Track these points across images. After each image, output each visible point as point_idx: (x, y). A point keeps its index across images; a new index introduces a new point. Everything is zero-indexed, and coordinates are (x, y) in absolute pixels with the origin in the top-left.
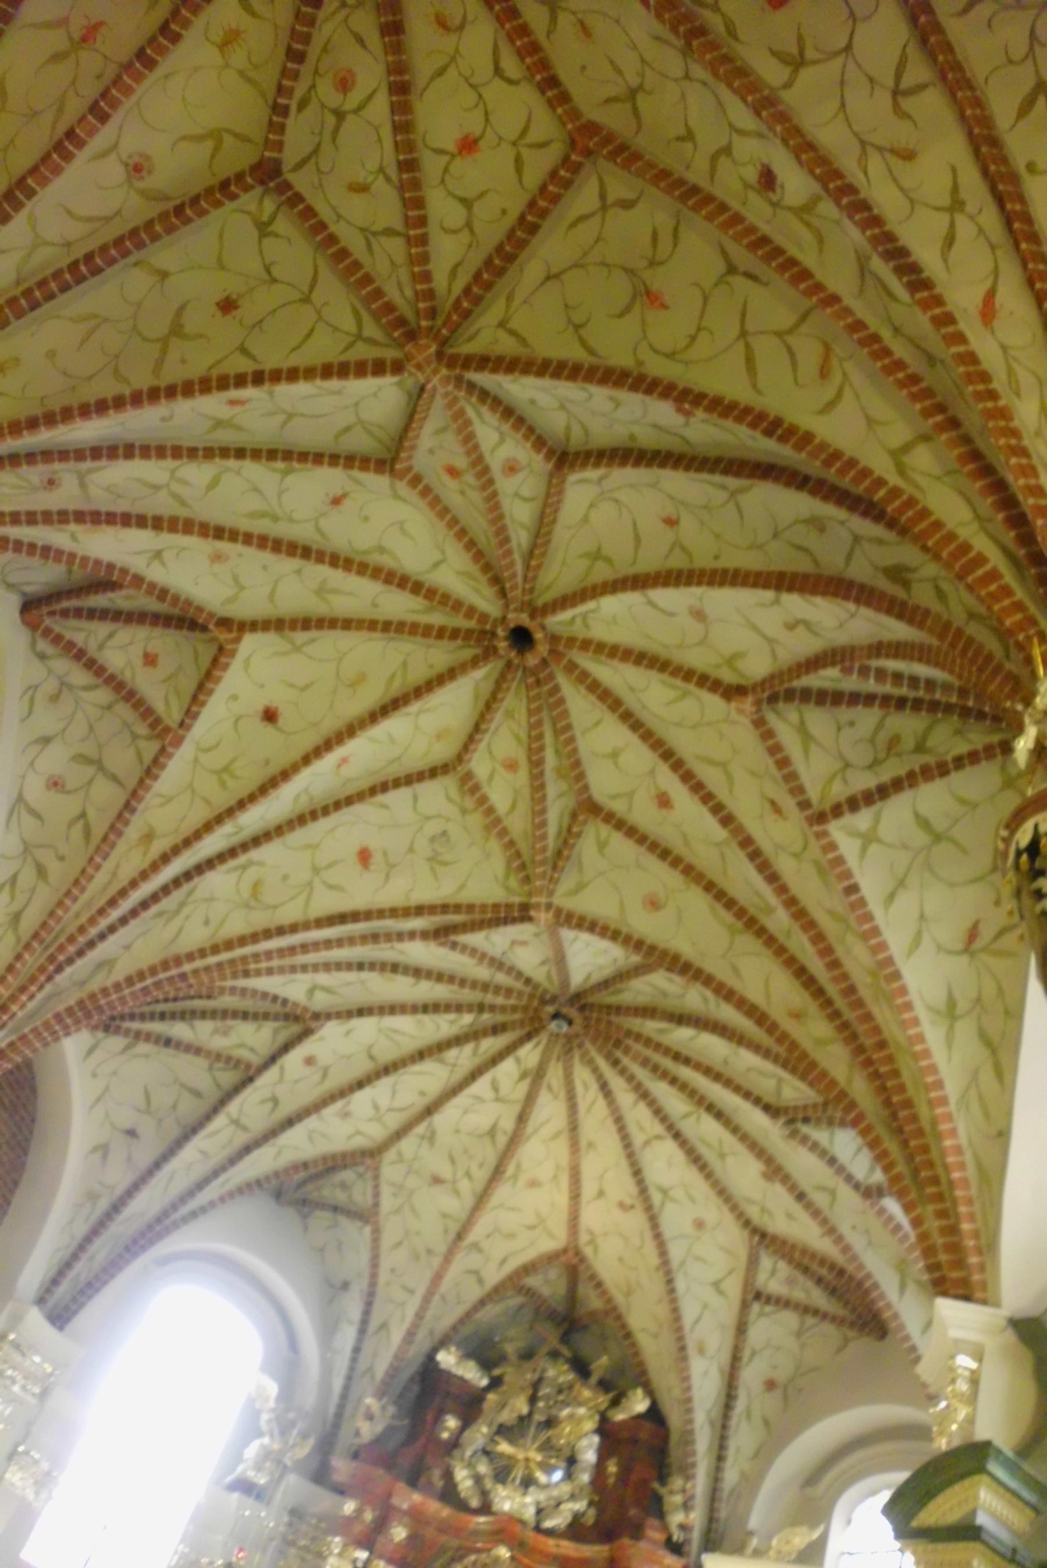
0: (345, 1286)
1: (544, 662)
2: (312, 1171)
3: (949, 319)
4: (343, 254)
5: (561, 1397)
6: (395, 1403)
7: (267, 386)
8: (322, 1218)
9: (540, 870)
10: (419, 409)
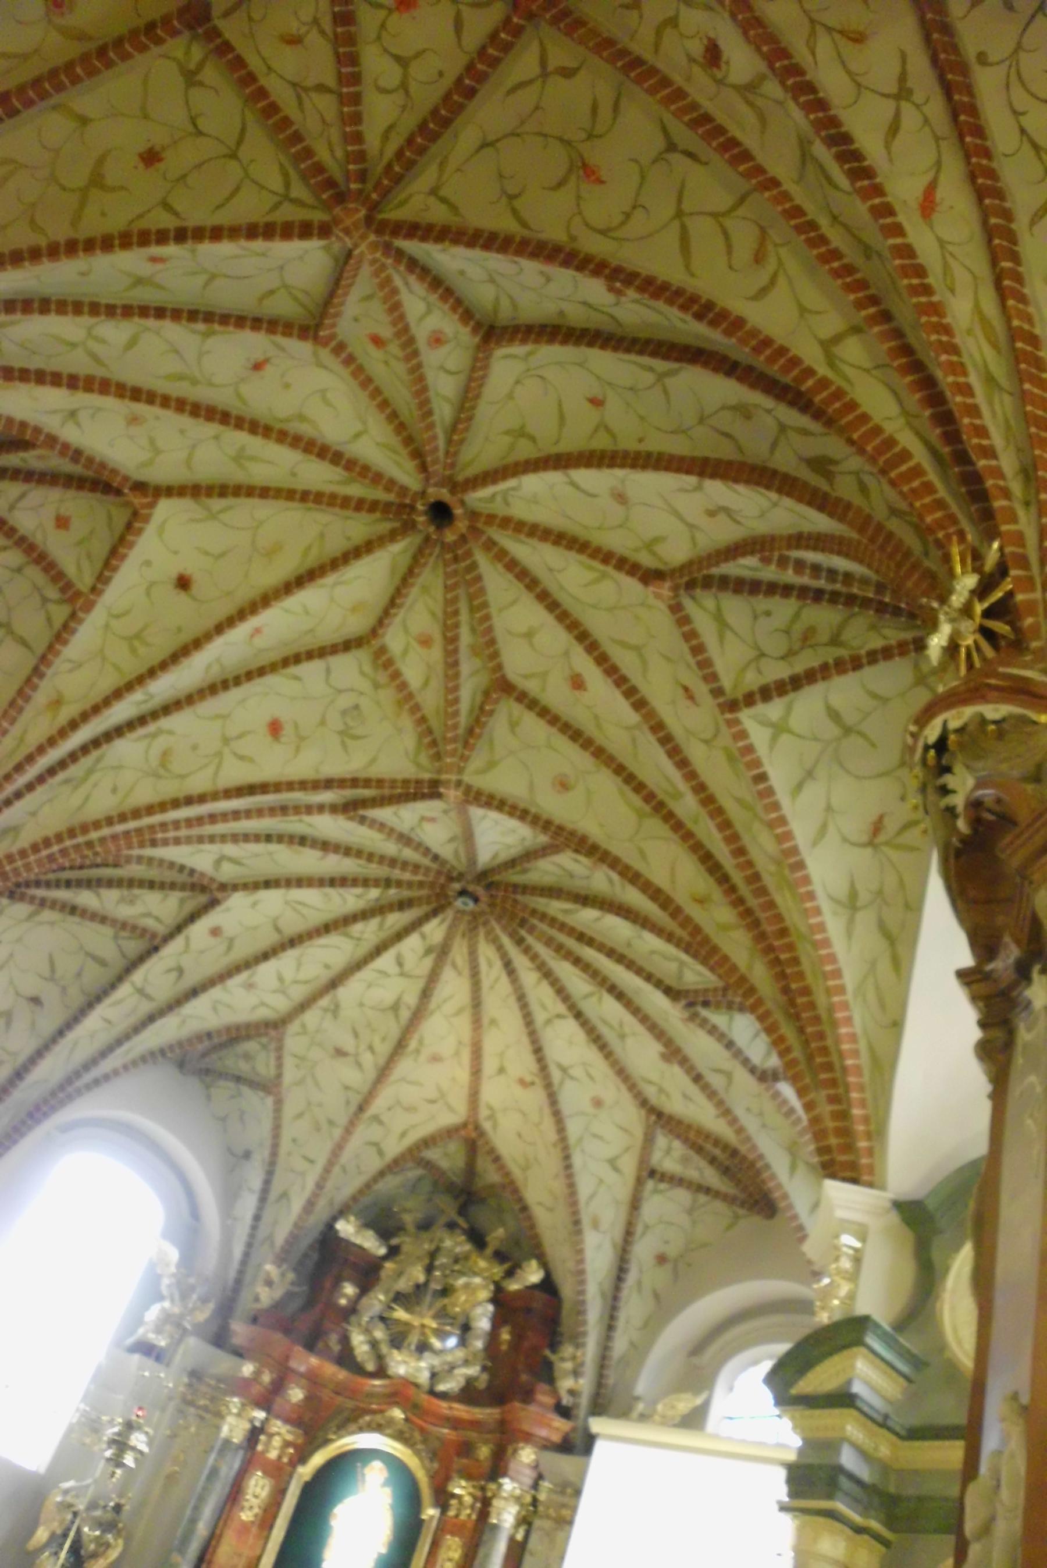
0: (247, 1155)
1: (463, 539)
2: (216, 1040)
3: (888, 210)
4: (272, 109)
5: (457, 1267)
6: (295, 1270)
7: (189, 245)
8: (223, 1089)
9: (449, 747)
10: (345, 275)
